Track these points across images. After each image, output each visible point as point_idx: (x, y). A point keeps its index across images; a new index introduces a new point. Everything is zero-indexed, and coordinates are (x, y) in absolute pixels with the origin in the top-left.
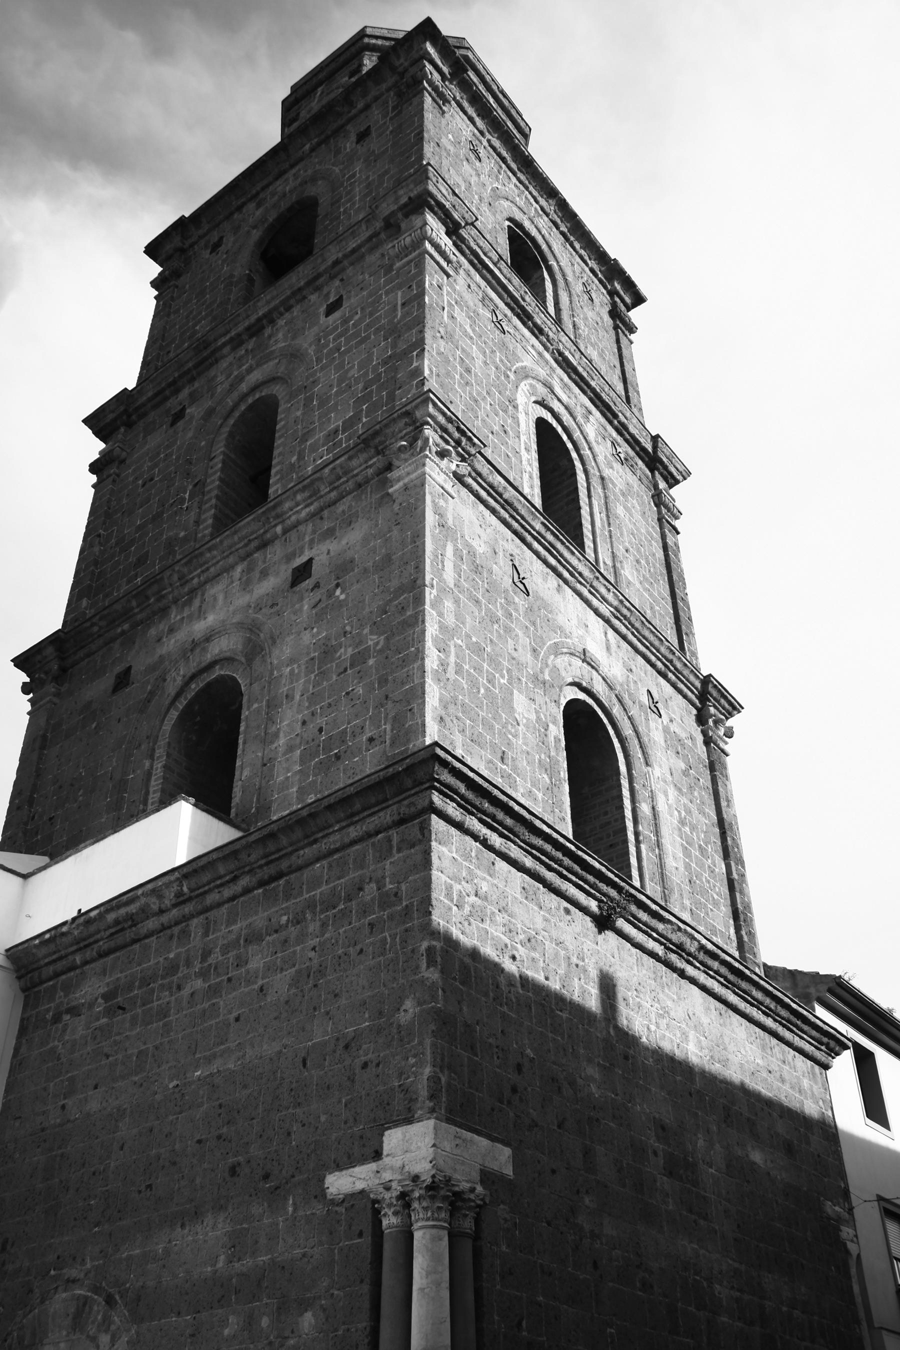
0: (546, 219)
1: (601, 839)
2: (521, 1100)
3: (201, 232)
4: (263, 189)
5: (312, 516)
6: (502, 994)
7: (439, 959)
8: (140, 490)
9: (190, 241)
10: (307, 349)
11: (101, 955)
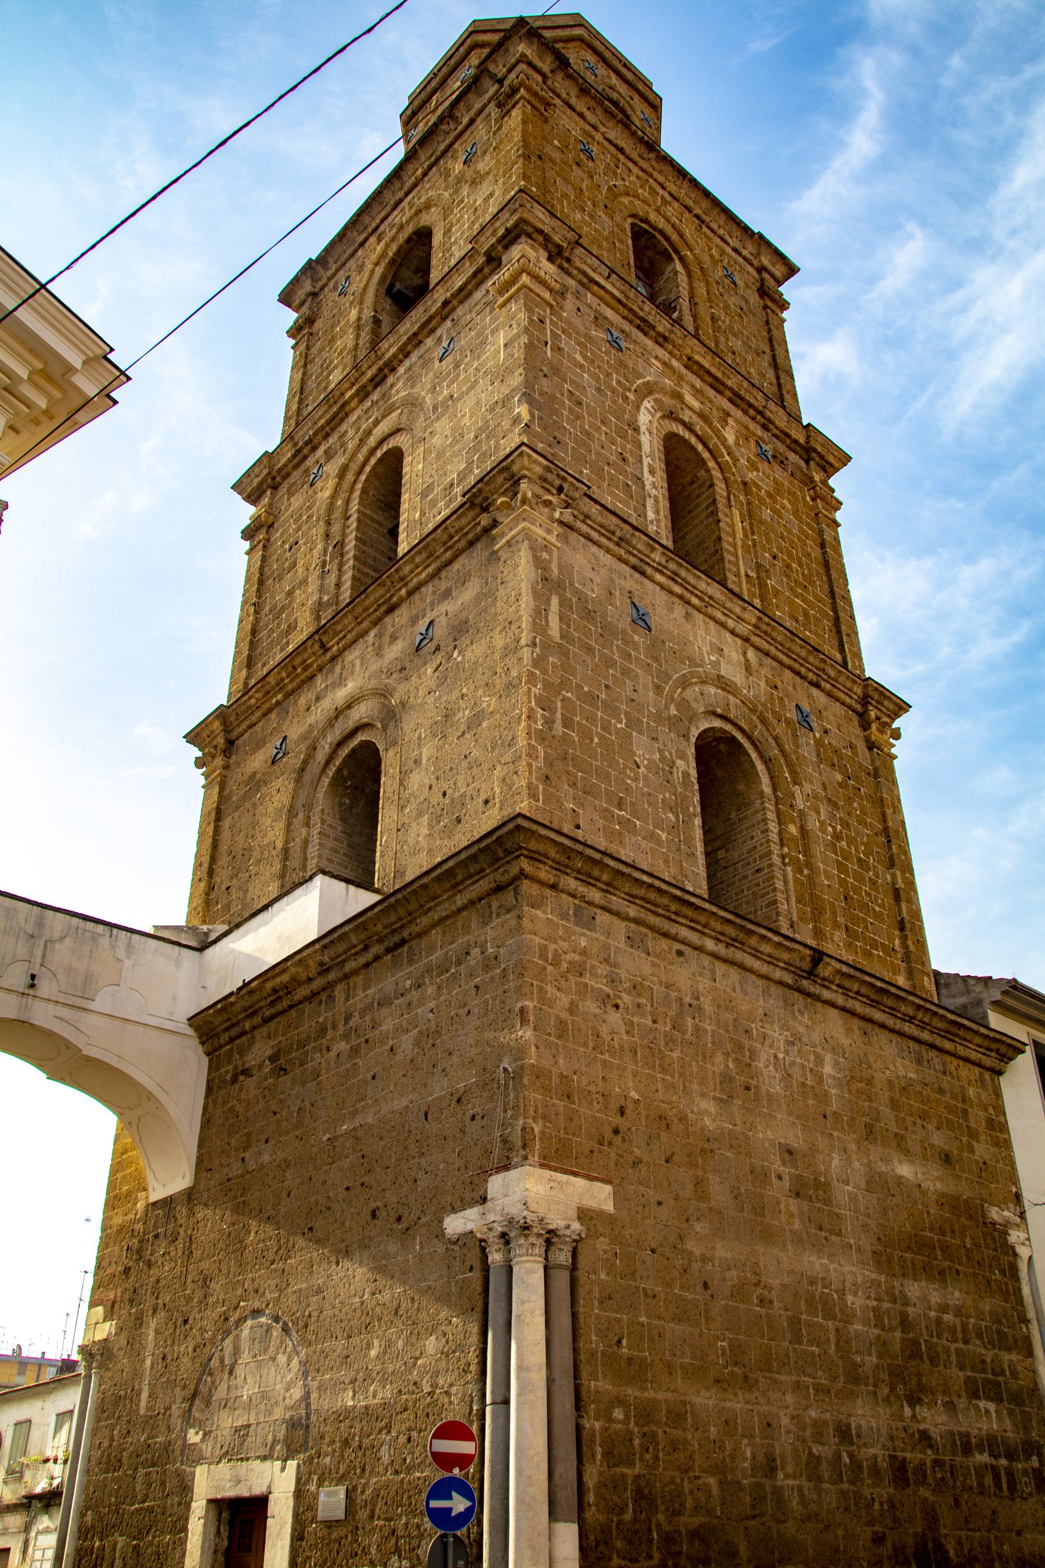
0: (676, 204)
1: (749, 864)
2: (624, 1140)
3: (330, 273)
4: (382, 221)
5: (433, 576)
6: (603, 1044)
7: (532, 1018)
8: (288, 554)
9: (321, 284)
10: (424, 397)
11: (266, 1021)
